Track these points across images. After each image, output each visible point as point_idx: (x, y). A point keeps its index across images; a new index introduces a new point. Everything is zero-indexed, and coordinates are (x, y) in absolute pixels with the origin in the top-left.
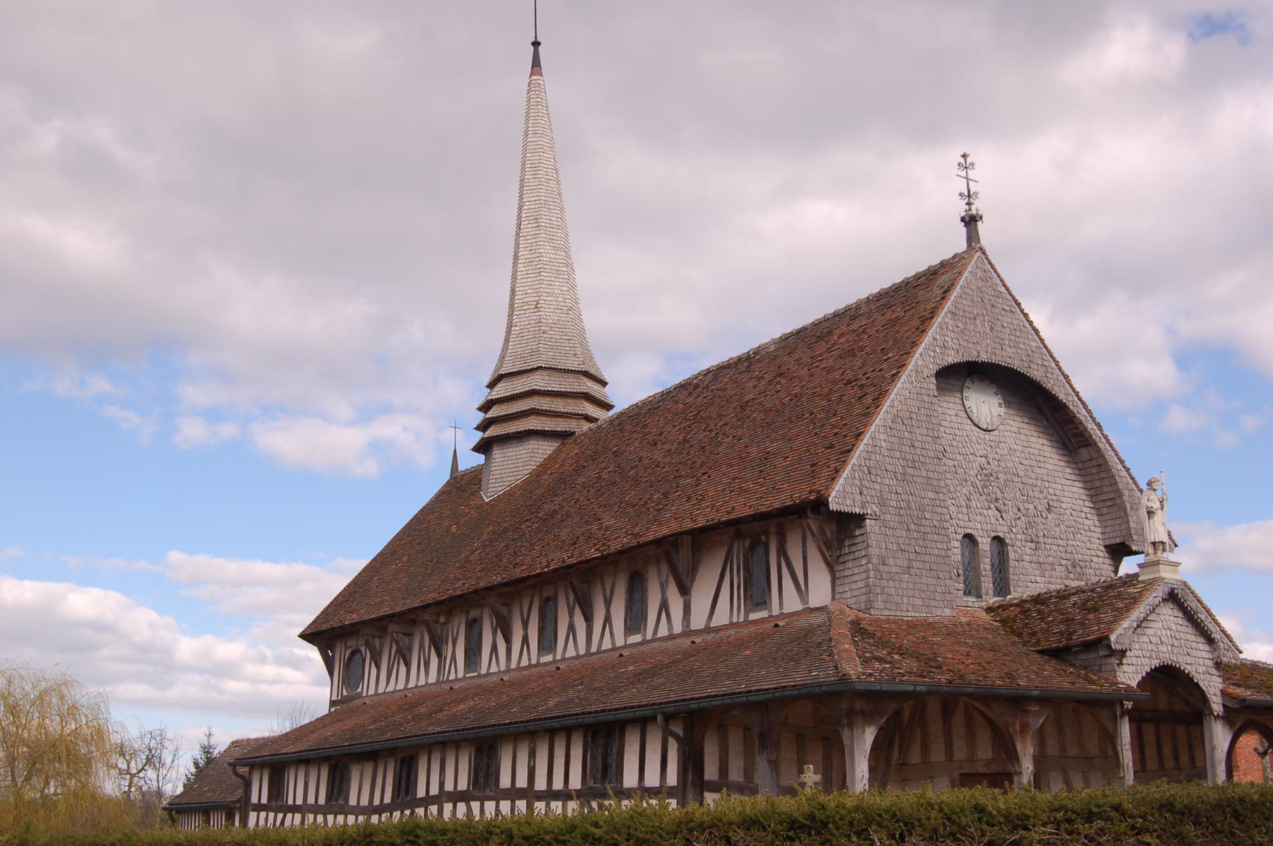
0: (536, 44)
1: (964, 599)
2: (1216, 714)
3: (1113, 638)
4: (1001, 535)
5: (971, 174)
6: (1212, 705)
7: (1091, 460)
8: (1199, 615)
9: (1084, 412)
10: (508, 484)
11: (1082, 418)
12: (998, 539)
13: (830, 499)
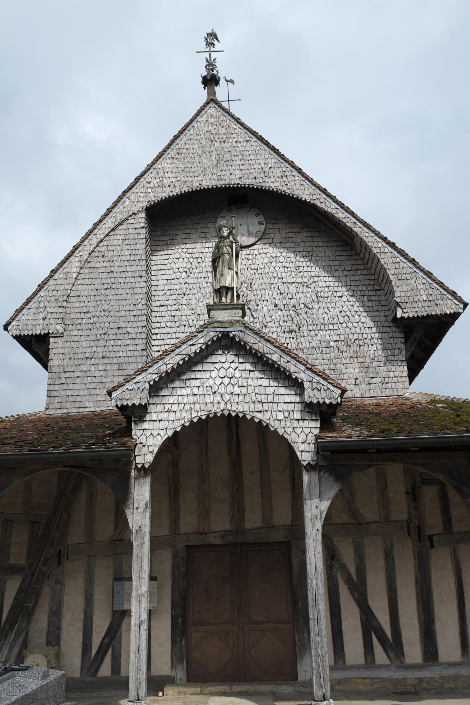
6: (299, 454)
8: (268, 356)
11: (333, 212)
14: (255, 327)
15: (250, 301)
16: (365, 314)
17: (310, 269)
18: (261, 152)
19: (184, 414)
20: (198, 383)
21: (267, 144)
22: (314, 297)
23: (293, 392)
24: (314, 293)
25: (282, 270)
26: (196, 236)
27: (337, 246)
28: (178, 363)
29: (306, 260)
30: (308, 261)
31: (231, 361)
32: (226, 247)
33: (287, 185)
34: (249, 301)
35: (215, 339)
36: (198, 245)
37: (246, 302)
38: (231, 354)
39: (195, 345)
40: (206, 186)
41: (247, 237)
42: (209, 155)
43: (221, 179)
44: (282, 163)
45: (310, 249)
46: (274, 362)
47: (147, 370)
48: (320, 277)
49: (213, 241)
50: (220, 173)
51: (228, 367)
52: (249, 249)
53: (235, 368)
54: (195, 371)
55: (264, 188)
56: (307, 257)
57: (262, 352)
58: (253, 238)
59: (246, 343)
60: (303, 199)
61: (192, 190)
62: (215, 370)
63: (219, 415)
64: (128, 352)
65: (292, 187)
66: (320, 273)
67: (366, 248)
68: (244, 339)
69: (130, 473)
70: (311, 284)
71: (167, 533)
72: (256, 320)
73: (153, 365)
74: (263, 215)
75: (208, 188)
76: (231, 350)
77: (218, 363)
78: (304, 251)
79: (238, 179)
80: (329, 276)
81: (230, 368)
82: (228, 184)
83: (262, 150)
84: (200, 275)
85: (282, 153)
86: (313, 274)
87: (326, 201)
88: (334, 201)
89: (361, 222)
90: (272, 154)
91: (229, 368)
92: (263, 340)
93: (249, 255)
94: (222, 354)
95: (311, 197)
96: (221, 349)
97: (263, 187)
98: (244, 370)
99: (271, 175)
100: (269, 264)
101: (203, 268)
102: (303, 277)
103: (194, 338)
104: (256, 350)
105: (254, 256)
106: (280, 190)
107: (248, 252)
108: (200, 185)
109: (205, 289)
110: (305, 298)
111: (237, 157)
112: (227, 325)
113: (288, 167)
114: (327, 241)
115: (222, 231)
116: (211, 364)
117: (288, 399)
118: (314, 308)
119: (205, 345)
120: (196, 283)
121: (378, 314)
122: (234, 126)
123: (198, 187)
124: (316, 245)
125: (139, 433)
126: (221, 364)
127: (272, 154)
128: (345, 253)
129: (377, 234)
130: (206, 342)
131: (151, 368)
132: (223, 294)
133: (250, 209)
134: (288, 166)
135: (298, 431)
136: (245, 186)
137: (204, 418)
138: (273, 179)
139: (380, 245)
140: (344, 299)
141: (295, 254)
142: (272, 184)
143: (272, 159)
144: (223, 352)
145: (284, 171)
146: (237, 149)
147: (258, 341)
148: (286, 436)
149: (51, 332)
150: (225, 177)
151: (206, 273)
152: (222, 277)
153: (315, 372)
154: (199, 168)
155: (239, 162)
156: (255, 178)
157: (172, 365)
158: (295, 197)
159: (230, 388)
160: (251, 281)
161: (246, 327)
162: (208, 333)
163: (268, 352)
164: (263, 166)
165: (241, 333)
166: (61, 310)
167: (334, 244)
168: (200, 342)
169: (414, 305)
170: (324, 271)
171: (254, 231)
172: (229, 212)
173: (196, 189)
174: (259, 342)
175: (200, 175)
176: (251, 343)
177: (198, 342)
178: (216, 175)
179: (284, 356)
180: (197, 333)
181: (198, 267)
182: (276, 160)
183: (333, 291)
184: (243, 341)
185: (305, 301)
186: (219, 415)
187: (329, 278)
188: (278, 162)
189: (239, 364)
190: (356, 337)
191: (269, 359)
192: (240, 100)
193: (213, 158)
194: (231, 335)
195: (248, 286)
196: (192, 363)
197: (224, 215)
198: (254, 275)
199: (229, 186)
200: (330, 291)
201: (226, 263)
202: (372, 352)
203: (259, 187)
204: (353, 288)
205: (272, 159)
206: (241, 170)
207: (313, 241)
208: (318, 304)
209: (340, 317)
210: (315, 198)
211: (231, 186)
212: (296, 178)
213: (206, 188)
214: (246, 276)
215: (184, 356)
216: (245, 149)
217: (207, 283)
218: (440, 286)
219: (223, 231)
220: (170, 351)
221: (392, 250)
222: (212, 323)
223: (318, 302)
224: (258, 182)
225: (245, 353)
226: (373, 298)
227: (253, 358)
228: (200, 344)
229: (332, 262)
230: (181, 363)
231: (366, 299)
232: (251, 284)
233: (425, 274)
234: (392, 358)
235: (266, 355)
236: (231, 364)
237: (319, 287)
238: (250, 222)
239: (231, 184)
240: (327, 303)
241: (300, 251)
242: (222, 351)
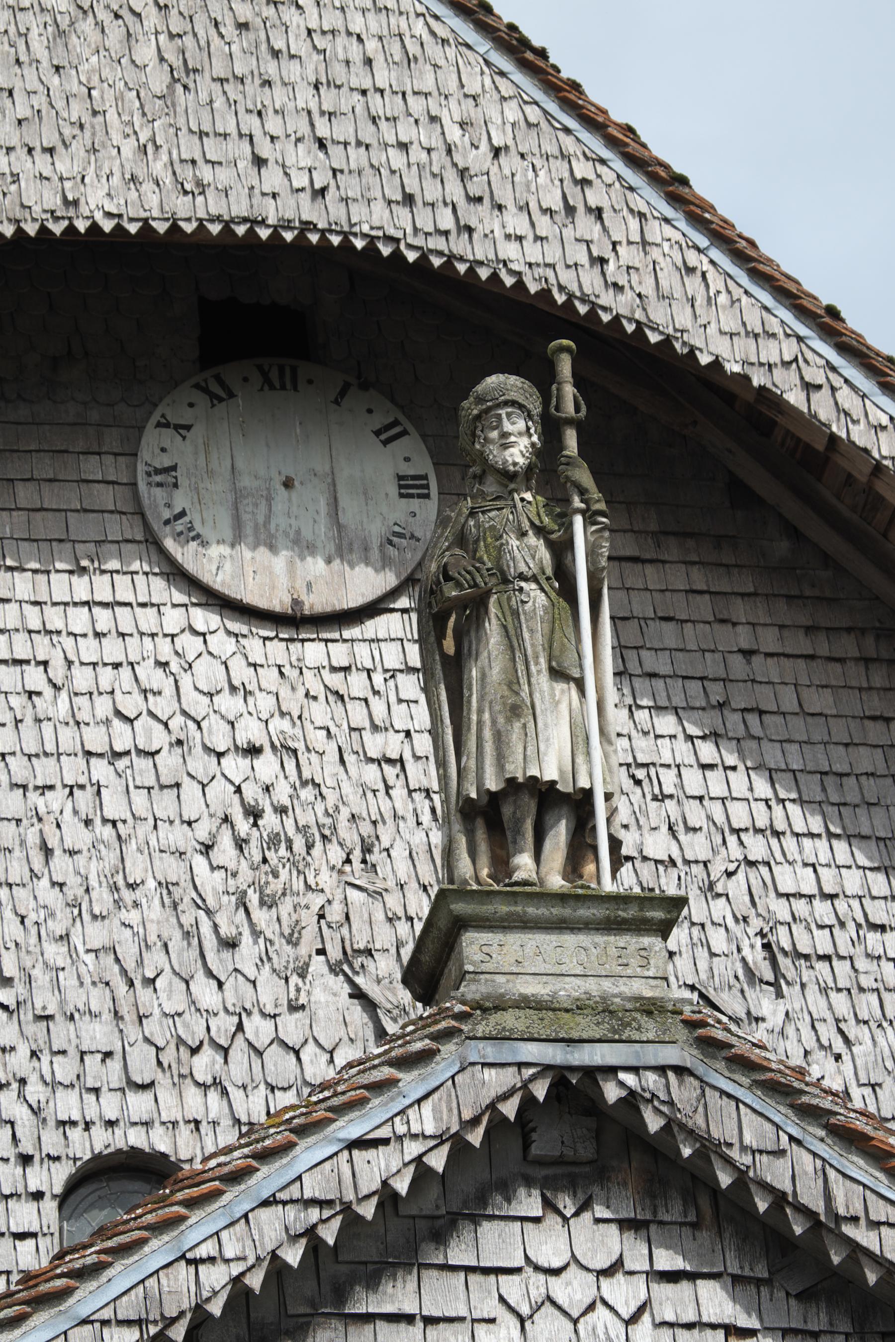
14: (763, 1047)
15: (369, 952)
17: (716, 784)
18: (434, 50)
22: (756, 956)
24: (751, 931)
27: (867, 661)
28: (274, 1255)
29: (693, 730)
30: (703, 738)
31: (602, 1262)
32: (523, 534)
33: (603, 261)
34: (358, 952)
35: (510, 1109)
37: (339, 955)
38: (598, 1221)
39: (385, 1142)
40: (109, 215)
41: (329, 561)
42: (115, 32)
43: (202, 187)
44: (567, 131)
45: (712, 666)
47: (64, 1294)
48: (777, 834)
49: (114, 564)
50: (189, 147)
51: (588, 1301)
52: (347, 634)
53: (633, 1309)
54: (369, 1318)
55: (462, 268)
56: (696, 714)
57: (819, 1206)
58: (370, 570)
60: (704, 359)
61: (20, 231)
62: (499, 1312)
65: (634, 277)
66: (778, 810)
68: (700, 1120)
70: (730, 874)
73: (109, 1265)
74: (424, 437)
75: (119, 229)
76: (596, 1190)
77: (517, 1270)
78: (675, 676)
79: (305, 198)
80: (831, 835)
81: (600, 1309)
82: (245, 220)
83: (444, 41)
84: (45, 772)
85: (564, 75)
86: (739, 815)
87: (837, 381)
90: (502, 74)
91: (591, 1307)
92: (822, 1133)
93: (346, 669)
94: (537, 1212)
95: (745, 347)
96: (529, 1182)
97: (461, 259)
98: (689, 1326)
99: (504, 195)
101: (61, 729)
102: (680, 828)
103: (376, 1102)
104: (779, 1199)
105: (378, 678)
106: (561, 288)
107: (340, 654)
108: (66, 202)
109: (81, 860)
110: (702, 954)
111: (295, 65)
112: (584, 1026)
113: (603, 162)
114: (810, 630)
115: (494, 434)
116: (474, 1279)
118: (757, 1020)
119: (445, 1148)
120: (18, 821)
123: (57, 219)
124: (745, 645)
126: (542, 1277)
127: (502, 74)
130: (455, 1128)
131: (92, 1285)
132: (518, 831)
133: (343, 393)
134: (606, 154)
136: (346, 245)
138: (517, 223)
141: (626, 691)
142: (510, 250)
143: (504, 99)
144: (549, 1205)
145: (584, 183)
147: (792, 1138)
150: (224, 176)
151: (81, 761)
152: (517, 725)
154: (60, 104)
155: (306, 97)
156: (409, 200)
157: (236, 1269)
158: (654, 338)
160: (366, 829)
162: (462, 1070)
163: (857, 1208)
164: (454, 134)
165: (681, 1082)
167: (847, 646)
168: (416, 1128)
170: (801, 801)
171: (376, 530)
172: (215, 398)
173: (43, 230)
174: (799, 1142)
175: (66, 146)
176: (744, 1148)
177: (401, 1129)
178: (165, 158)
180: (391, 1063)
181: (29, 720)
182: (528, 109)
183: (859, 926)
184: (691, 1133)
185: (703, 976)
187: (835, 843)
188: (544, 125)
189: (654, 1286)
191: (864, 1260)
193: (146, 53)
194: (612, 1093)
195: (348, 861)
196: (344, 1269)
197: (185, 416)
198: (381, 794)
199: (251, 232)
200: (842, 924)
203: (437, 262)
205: (504, 99)
206: (322, 144)
207: (723, 621)
208: (779, 995)
210: (775, 358)
211: (264, 233)
212: (655, 231)
213: (107, 226)
214: (332, 798)
215: (314, 1214)
216: (339, 25)
217: (88, 822)
219: (505, 435)
220: (221, 1179)
222: (485, 1010)
223: (776, 985)
224: (430, 229)
225: (692, 1218)
227: (739, 1250)
228: (414, 1137)
229: (841, 749)
230: (293, 1256)
232: (367, 849)
235: (848, 1230)
236: (605, 1283)
237: (780, 895)
238: (347, 471)
239: (263, 223)
240: (833, 995)
241: (652, 675)
242: (536, 1193)
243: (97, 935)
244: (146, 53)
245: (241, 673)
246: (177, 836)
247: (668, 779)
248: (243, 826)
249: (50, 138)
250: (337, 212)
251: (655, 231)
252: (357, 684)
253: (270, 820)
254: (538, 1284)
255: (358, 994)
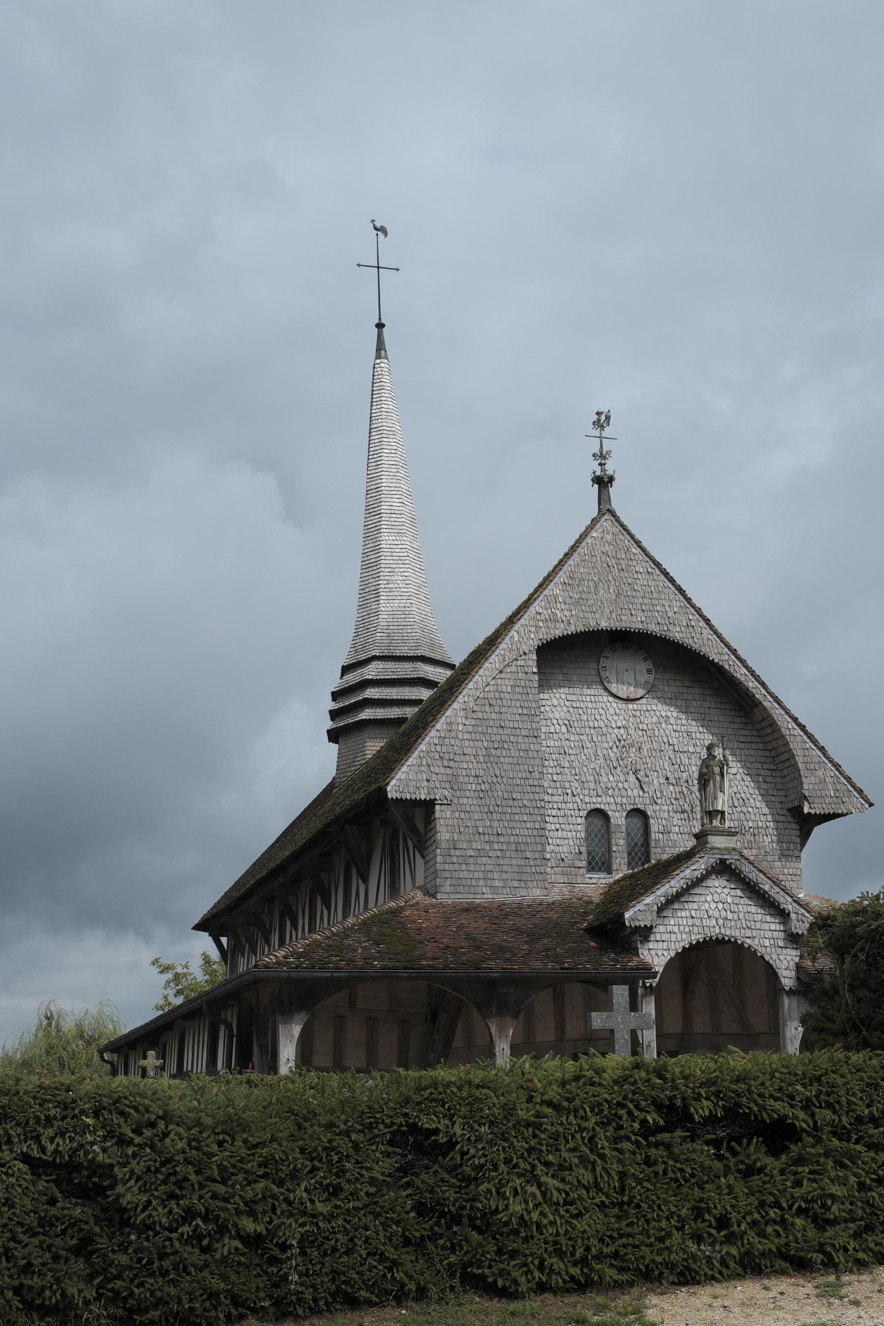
0: (380, 326)
1: (587, 876)
2: (787, 989)
3: (627, 915)
4: (641, 807)
5: (608, 432)
6: (782, 979)
7: (764, 719)
8: (761, 886)
9: (744, 670)
10: (349, 774)
11: (743, 679)
12: (638, 814)
13: (389, 788)
16: (760, 798)
19: (684, 936)
20: (695, 906)
21: (672, 581)
23: (777, 921)
25: (673, 734)
26: (575, 678)
36: (578, 691)
45: (702, 710)
46: (765, 891)
59: (741, 871)
63: (714, 938)
64: (526, 830)
67: (773, 724)
69: (637, 990)
71: (552, 1039)
72: (646, 795)
88: (744, 666)
89: (771, 696)
99: (676, 622)
100: (658, 725)
107: (635, 707)
117: (773, 927)
121: (773, 799)
122: (634, 551)
125: (646, 953)
128: (739, 720)
129: (788, 712)
135: (782, 958)
137: (701, 940)
138: (678, 629)
139: (790, 727)
140: (738, 777)
142: (677, 635)
146: (638, 581)
148: (771, 961)
149: (437, 797)
153: (801, 905)
159: (723, 913)
161: (742, 856)
164: (667, 608)
166: (448, 771)
167: (727, 706)
169: (822, 800)
171: (643, 681)
179: (775, 887)
186: (714, 938)
190: (751, 824)
192: (397, 270)
201: (718, 785)
202: (767, 844)
204: (748, 765)
209: (735, 799)
218: (848, 781)
221: (802, 734)
226: (769, 779)
231: (761, 780)
233: (834, 766)
234: (787, 852)
243: (592, 765)
244: (612, 591)
245: (618, 711)
246: (605, 745)
247: (694, 735)
248: (618, 744)
249: (595, 610)
250: (646, 626)
251: (704, 631)
252: (638, 713)
253: (622, 742)
254: (715, 889)
255: (637, 778)
